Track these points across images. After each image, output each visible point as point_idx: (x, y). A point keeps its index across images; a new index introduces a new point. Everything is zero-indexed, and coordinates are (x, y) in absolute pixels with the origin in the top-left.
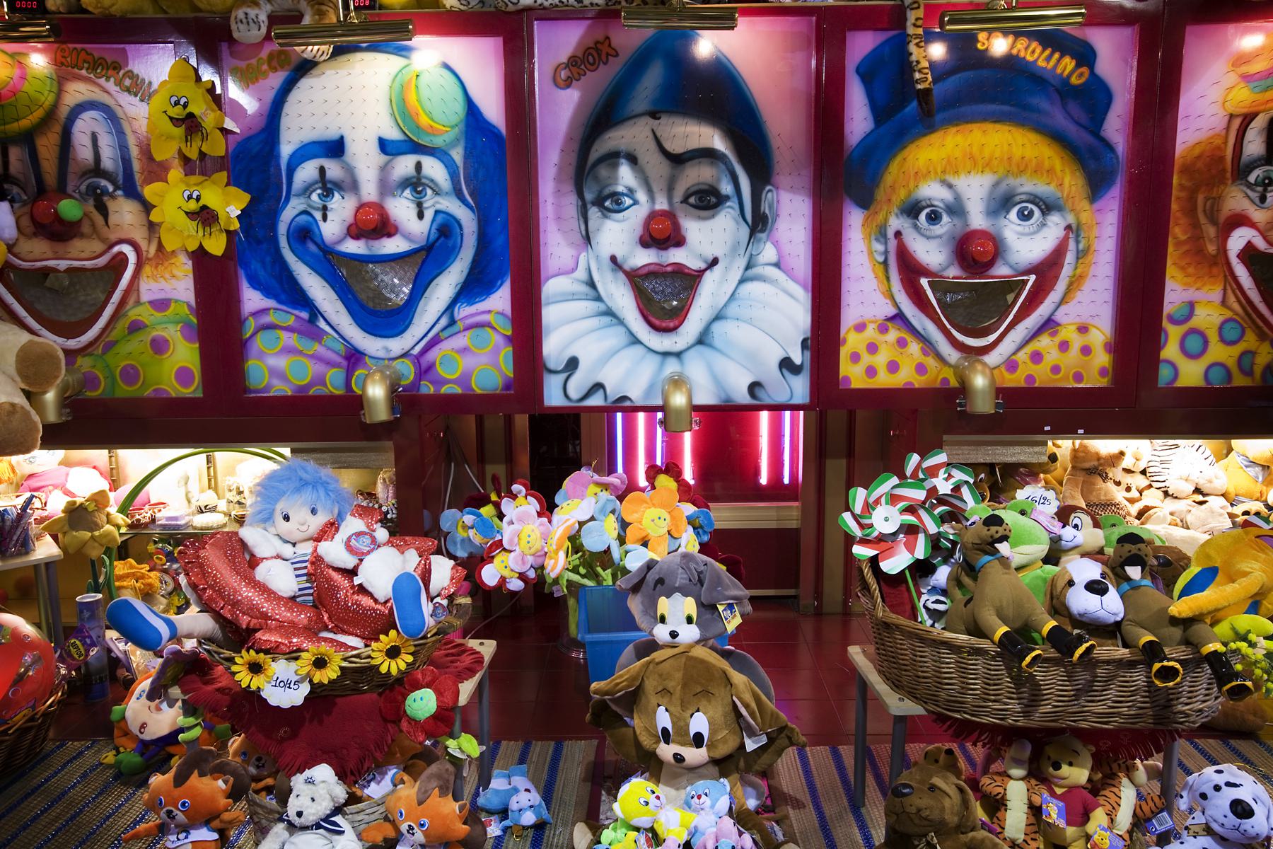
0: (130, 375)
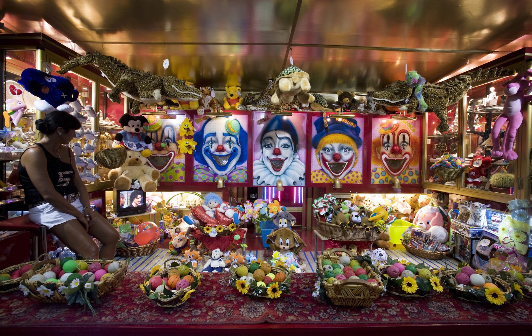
0: (171, 177)
